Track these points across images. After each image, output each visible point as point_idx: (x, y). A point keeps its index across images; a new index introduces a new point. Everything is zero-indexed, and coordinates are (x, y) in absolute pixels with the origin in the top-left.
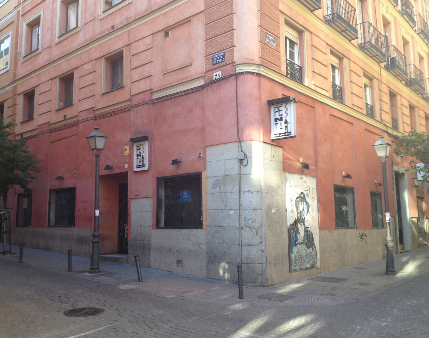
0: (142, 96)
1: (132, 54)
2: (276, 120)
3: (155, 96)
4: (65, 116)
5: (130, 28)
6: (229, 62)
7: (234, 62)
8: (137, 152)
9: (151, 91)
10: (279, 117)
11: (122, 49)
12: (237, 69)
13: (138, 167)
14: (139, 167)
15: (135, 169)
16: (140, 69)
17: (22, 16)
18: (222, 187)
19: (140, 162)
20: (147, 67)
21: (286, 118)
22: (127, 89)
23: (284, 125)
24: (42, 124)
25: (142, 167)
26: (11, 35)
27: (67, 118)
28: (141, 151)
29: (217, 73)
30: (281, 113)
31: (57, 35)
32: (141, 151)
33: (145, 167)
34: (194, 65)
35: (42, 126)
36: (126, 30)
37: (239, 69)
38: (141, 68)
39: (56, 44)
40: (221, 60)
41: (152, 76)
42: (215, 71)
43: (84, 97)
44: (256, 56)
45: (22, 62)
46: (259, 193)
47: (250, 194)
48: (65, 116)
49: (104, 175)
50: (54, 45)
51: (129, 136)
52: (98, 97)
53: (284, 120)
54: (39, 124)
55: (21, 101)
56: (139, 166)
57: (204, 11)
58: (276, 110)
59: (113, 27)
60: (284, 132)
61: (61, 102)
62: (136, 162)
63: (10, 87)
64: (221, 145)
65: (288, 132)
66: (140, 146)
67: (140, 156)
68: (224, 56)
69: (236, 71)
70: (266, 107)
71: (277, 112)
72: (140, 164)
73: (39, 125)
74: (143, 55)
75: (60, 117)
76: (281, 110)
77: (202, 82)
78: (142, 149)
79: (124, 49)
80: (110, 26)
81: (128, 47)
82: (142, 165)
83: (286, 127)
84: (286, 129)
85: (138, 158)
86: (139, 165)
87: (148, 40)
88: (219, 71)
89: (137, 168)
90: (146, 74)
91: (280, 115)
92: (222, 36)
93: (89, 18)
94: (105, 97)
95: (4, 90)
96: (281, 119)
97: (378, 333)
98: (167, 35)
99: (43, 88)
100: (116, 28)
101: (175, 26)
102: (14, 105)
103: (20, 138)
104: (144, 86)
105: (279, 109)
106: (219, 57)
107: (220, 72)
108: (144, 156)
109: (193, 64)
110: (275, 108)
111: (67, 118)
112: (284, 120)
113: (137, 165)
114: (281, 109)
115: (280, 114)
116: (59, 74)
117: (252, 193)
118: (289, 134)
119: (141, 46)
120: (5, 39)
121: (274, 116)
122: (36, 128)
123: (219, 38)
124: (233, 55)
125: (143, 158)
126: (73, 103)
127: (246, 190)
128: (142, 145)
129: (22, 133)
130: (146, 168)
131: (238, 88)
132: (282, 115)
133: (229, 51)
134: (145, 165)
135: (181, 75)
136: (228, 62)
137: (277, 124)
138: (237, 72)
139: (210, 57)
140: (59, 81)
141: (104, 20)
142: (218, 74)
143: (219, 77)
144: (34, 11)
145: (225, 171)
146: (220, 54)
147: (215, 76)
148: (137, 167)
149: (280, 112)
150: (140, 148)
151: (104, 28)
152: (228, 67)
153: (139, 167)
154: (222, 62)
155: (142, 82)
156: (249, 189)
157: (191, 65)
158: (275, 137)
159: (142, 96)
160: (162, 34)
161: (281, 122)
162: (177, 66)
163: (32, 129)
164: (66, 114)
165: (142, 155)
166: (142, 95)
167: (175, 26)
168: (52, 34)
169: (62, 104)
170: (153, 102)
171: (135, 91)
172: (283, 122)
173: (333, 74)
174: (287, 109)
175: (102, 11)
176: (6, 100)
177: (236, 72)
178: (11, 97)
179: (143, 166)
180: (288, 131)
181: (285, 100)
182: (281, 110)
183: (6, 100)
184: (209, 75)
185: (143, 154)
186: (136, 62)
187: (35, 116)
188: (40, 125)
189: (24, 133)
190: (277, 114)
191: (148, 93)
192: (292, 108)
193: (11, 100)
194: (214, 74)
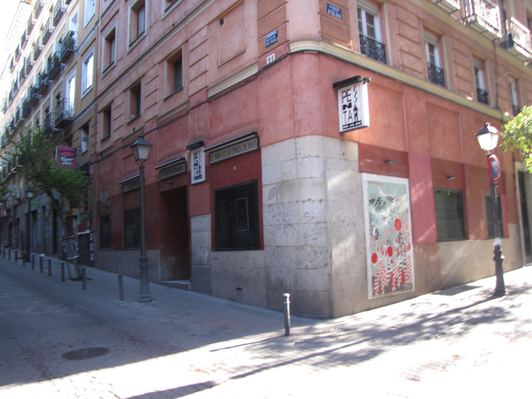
0: (198, 96)
1: (189, 50)
2: (344, 107)
3: (211, 94)
5: (187, 22)
6: (282, 41)
7: (288, 41)
8: (194, 162)
9: (207, 89)
10: (347, 104)
11: (181, 47)
12: (291, 48)
14: (196, 178)
15: (194, 182)
16: (196, 66)
17: (101, 31)
18: (278, 196)
19: (197, 172)
20: (203, 62)
22: (185, 90)
23: (353, 113)
24: (117, 140)
26: (94, 52)
27: (136, 130)
28: (198, 159)
29: (271, 56)
30: (349, 98)
31: (128, 44)
33: (201, 178)
34: (248, 51)
35: (117, 142)
36: (184, 25)
37: (295, 47)
38: (197, 64)
39: (128, 54)
40: (274, 41)
41: (207, 71)
42: (268, 54)
44: (314, 29)
45: (101, 78)
46: (323, 202)
47: (310, 203)
48: (134, 129)
50: (126, 55)
51: (187, 144)
52: (161, 102)
53: (353, 107)
55: (101, 118)
56: (197, 177)
58: (344, 94)
59: (174, 25)
60: (354, 121)
62: (193, 174)
63: (93, 106)
64: (277, 144)
65: (357, 122)
66: (197, 154)
67: (350, 106)
68: (277, 35)
69: (290, 50)
70: (331, 92)
73: (114, 142)
74: (199, 50)
76: (350, 95)
77: (254, 70)
79: (183, 46)
80: (171, 24)
81: (186, 44)
82: (199, 176)
84: (356, 116)
85: (345, 112)
86: (347, 123)
87: (204, 32)
88: (272, 53)
90: (202, 70)
91: (348, 101)
92: (274, 13)
93: (153, 21)
95: (89, 109)
98: (222, 22)
99: (117, 102)
100: (175, 25)
101: (229, 10)
104: (200, 84)
105: (347, 93)
106: (272, 37)
107: (274, 55)
108: (201, 165)
109: (247, 50)
110: (343, 92)
111: (136, 130)
112: (353, 107)
113: (344, 124)
114: (349, 93)
116: (129, 85)
117: (313, 201)
118: (360, 123)
119: (197, 40)
120: (90, 57)
121: (342, 103)
123: (271, 15)
124: (286, 32)
125: (200, 167)
127: (306, 199)
128: (198, 153)
131: (190, 39)
132: (350, 100)
133: (282, 29)
135: (235, 65)
136: (281, 41)
138: (292, 51)
139: (262, 39)
141: (166, 19)
142: (271, 58)
143: (273, 60)
144: (111, 23)
145: (282, 177)
146: (274, 33)
147: (269, 60)
150: (197, 156)
151: (166, 28)
152: (282, 47)
153: (196, 178)
154: (275, 42)
155: (199, 80)
156: (309, 197)
157: (245, 51)
158: (344, 129)
159: (198, 96)
160: (218, 22)
162: (232, 55)
164: (135, 127)
165: (199, 164)
166: (199, 94)
167: (229, 10)
168: (125, 45)
170: (210, 101)
171: (192, 91)
172: (352, 109)
173: (370, 25)
175: (164, 10)
177: (290, 51)
179: (200, 177)
180: (358, 119)
181: (354, 81)
184: (262, 60)
185: (200, 162)
186: (193, 59)
188: (116, 141)
189: (103, 151)
191: (204, 91)
192: (364, 89)
194: (268, 58)
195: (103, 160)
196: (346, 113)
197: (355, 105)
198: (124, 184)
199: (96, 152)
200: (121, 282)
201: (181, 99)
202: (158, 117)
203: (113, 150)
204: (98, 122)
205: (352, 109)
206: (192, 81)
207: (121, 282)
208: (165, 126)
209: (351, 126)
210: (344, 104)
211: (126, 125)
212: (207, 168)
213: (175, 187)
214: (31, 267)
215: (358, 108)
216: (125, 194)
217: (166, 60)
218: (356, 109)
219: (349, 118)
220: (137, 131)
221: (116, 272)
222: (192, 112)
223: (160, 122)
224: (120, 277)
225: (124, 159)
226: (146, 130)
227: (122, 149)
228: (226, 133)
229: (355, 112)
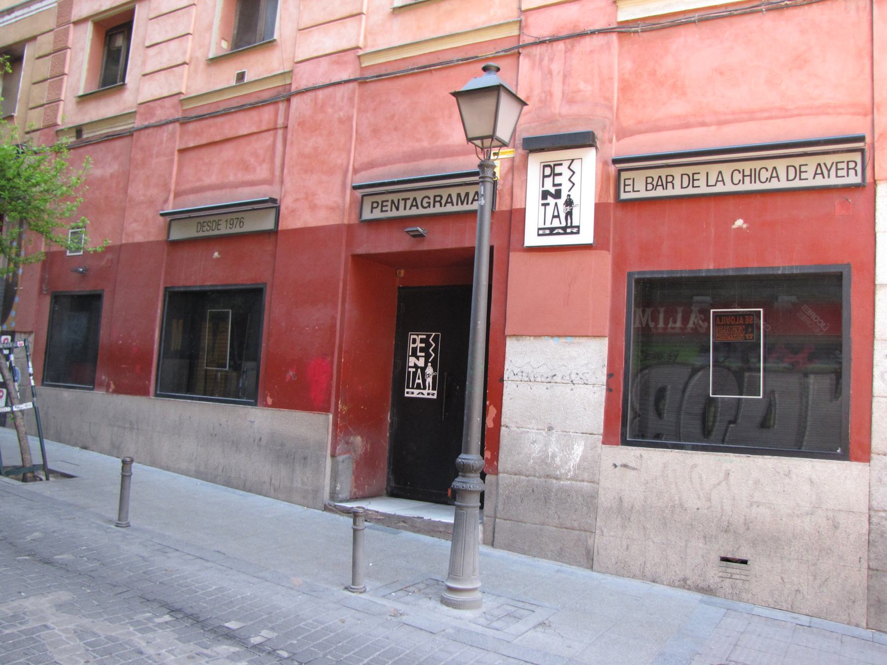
4: (241, 76)
10: (553, 190)
13: (548, 232)
15: (531, 239)
21: (569, 193)
25: (565, 233)
30: (558, 180)
32: (562, 180)
33: (578, 233)
35: (152, 104)
41: (361, 14)
43: (322, 17)
49: (361, 255)
53: (564, 197)
54: (141, 100)
57: (49, 81)
61: (223, 39)
65: (572, 227)
67: (557, 195)
71: (549, 176)
72: (556, 223)
75: (225, 77)
76: (560, 174)
78: (567, 174)
82: (564, 229)
83: (569, 214)
85: (545, 205)
86: (548, 225)
89: (539, 235)
94: (398, 23)
96: (557, 195)
97: (248, 613)
102: (60, 50)
103: (74, 139)
105: (553, 170)
112: (564, 197)
113: (542, 226)
115: (556, 182)
122: (134, 110)
126: (276, 36)
129: (83, 125)
130: (586, 236)
132: (560, 185)
134: (578, 227)
137: (548, 204)
140: (93, 40)
148: (541, 232)
149: (556, 178)
153: (544, 232)
161: (558, 201)
163: (115, 115)
169: (224, 45)
171: (146, 96)
174: (574, 173)
176: (34, 38)
178: (52, 28)
180: (571, 223)
182: (560, 174)
183: (34, 38)
187: (131, 78)
190: (549, 182)
193: (50, 37)
195: (79, 147)
196: (547, 207)
197: (569, 195)
198: (174, 218)
199: (56, 125)
200: (125, 476)
201: (108, 108)
202: (183, 97)
203: (138, 123)
204: (70, 46)
205: (561, 202)
206: (162, 72)
207: (125, 476)
208: (392, 78)
209: (555, 232)
210: (545, 188)
211: (74, 100)
212: (600, 208)
213: (424, 247)
214: (506, 429)
215: (576, 201)
216: (175, 244)
217: (92, 21)
218: (569, 203)
219: (554, 217)
220: (247, 83)
221: (114, 450)
222: (537, 50)
223: (366, 67)
224: (126, 464)
225: (182, 151)
226: (302, 81)
227: (177, 125)
228: (703, 124)
229: (568, 208)
